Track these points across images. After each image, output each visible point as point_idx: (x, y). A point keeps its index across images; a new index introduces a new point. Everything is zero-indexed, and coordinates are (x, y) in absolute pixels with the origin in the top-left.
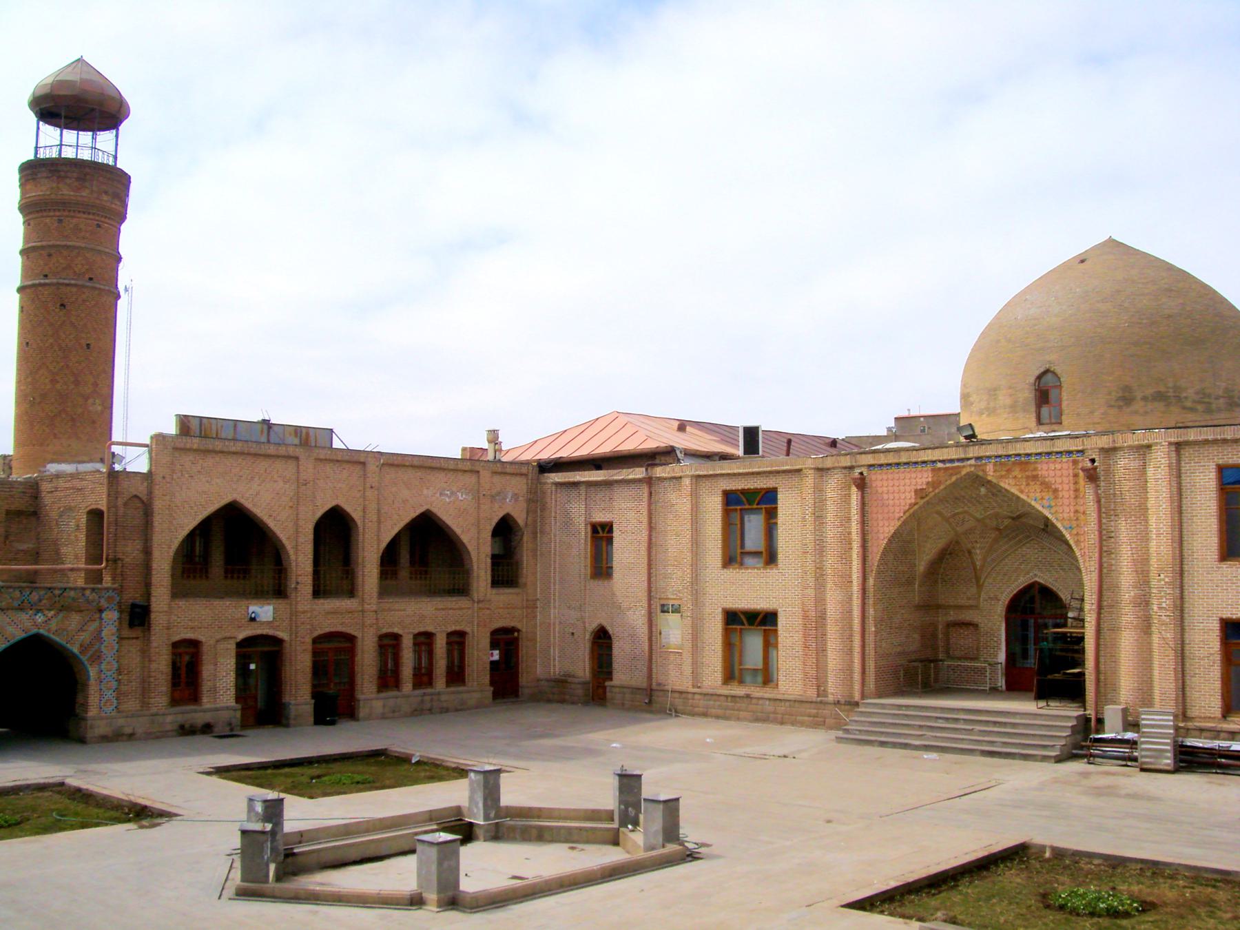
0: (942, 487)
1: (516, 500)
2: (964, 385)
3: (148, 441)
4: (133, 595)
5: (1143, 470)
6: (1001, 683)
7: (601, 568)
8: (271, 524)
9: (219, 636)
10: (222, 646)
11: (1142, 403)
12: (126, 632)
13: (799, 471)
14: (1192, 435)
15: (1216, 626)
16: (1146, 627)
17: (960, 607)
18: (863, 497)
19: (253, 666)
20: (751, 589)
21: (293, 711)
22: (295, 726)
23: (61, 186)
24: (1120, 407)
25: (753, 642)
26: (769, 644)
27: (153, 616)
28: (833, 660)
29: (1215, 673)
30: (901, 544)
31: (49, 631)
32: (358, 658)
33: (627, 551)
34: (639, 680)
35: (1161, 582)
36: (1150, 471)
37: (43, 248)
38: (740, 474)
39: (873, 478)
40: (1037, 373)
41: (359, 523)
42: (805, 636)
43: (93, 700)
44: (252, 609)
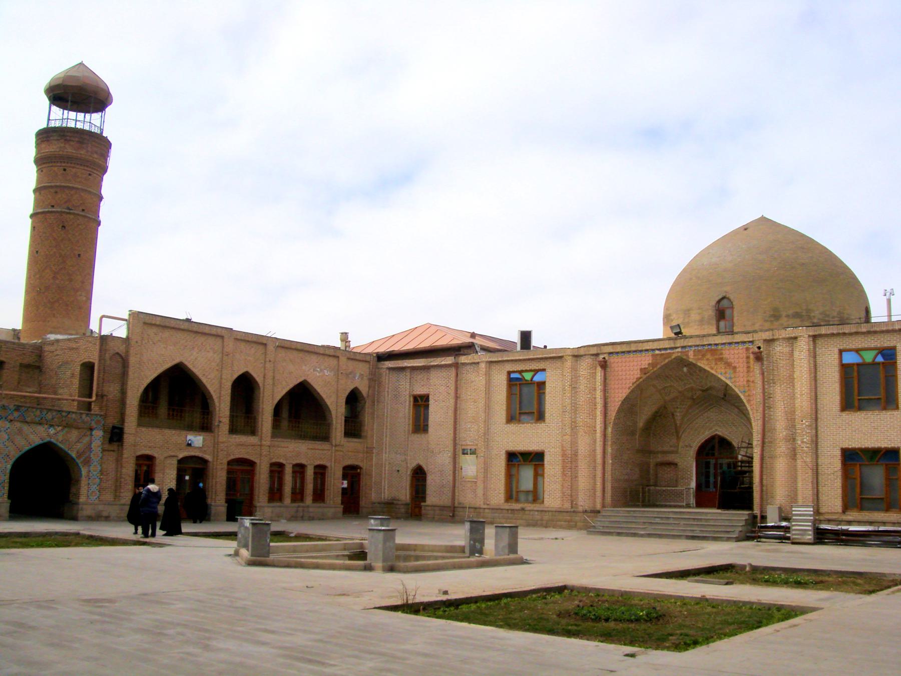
0: (659, 366)
1: (362, 379)
2: (666, 308)
3: (127, 317)
4: (112, 421)
5: (791, 354)
6: (693, 501)
7: (420, 425)
8: (204, 380)
9: (166, 455)
10: (168, 461)
11: (786, 319)
12: (107, 446)
13: (561, 357)
14: (823, 330)
15: (838, 453)
16: (793, 455)
17: (664, 452)
18: (605, 375)
19: (187, 478)
20: (526, 437)
21: (213, 510)
22: (215, 520)
23: (67, 146)
24: (771, 321)
25: (526, 475)
26: (538, 473)
27: (125, 436)
28: (583, 482)
29: (838, 483)
30: (629, 406)
31: (57, 440)
32: (257, 477)
33: (438, 413)
34: (446, 500)
35: (803, 425)
36: (796, 354)
37: (51, 187)
38: (520, 360)
39: (612, 361)
40: (717, 299)
41: (261, 385)
42: (563, 468)
43: (84, 490)
44: (190, 437)
